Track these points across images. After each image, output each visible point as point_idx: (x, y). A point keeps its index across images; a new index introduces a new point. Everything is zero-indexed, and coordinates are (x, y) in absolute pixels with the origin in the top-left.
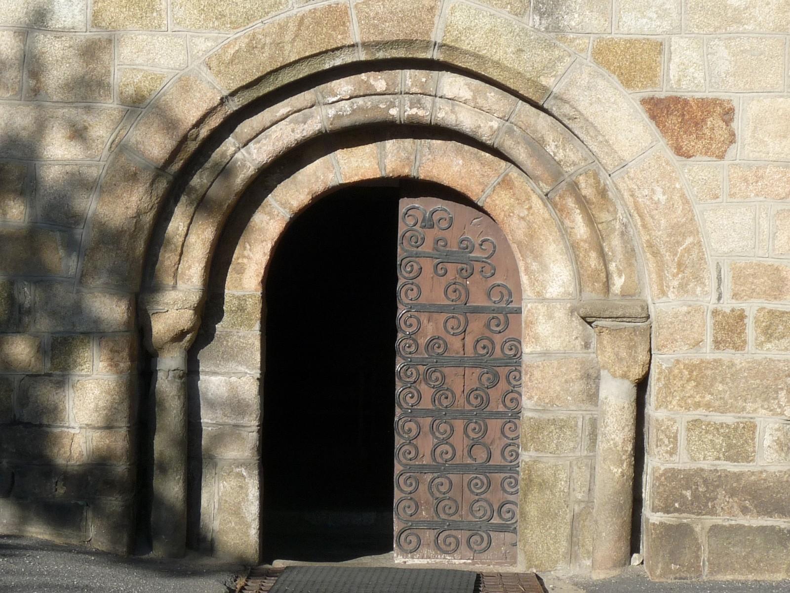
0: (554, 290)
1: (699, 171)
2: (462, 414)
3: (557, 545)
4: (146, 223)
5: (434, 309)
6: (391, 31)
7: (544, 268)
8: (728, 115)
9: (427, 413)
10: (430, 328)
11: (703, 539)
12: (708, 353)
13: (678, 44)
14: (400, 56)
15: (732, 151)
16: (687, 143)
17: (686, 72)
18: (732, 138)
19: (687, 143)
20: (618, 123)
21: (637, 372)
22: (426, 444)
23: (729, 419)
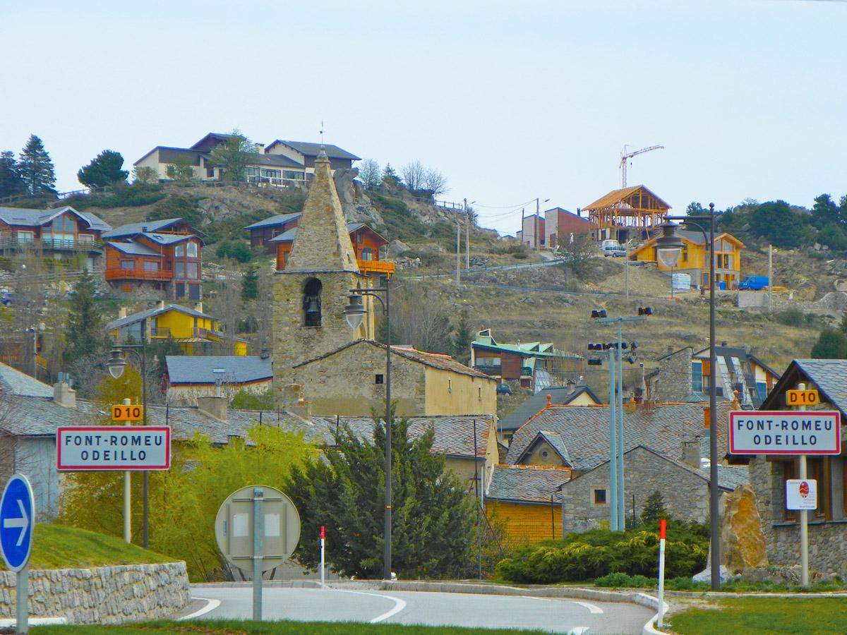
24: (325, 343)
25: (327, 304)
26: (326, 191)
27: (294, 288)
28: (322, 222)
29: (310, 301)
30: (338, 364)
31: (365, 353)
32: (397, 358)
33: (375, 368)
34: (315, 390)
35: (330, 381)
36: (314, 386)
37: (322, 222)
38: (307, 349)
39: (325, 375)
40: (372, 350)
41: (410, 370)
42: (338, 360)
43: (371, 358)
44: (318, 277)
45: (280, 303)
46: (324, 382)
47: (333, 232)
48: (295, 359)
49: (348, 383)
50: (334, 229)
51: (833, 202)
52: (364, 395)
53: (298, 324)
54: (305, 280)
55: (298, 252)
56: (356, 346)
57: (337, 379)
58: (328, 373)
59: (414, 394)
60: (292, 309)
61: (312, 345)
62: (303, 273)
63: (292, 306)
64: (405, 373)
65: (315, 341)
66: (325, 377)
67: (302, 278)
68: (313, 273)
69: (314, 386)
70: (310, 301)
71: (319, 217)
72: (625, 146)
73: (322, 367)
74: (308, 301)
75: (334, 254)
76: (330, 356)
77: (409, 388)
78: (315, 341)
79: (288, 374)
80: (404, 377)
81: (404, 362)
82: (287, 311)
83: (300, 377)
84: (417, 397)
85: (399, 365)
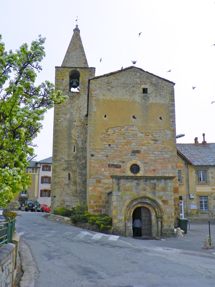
0: (154, 215)
1: (166, 206)
2: (146, 225)
3: (104, 101)
4: (109, 216)
5: (144, 216)
6: (143, 195)
7: (153, 213)
8: (168, 201)
9: (144, 225)
10: (144, 218)
11: (167, 234)
12: (167, 220)
13: (164, 196)
14: (142, 230)
15: (168, 204)
16: (165, 204)
17: (164, 198)
18: (168, 203)
19: (165, 204)
20: (161, 203)
21: (161, 221)
22: (144, 227)
23: (169, 225)
24: (81, 100)
25: (83, 82)
26: (79, 40)
27: (66, 74)
28: (78, 51)
29: (73, 81)
30: (118, 80)
31: (136, 75)
32: (156, 79)
33: (142, 84)
34: (104, 95)
35: (114, 90)
36: (103, 92)
37: (78, 51)
38: (72, 102)
39: (110, 86)
40: (140, 73)
41: (165, 87)
42: (118, 77)
43: (140, 78)
44: (78, 70)
45: (59, 80)
46: (109, 90)
47: (83, 55)
48: (66, 106)
49: (125, 91)
50: (84, 54)
51: (195, 170)
52: (136, 100)
53: (68, 90)
54: (72, 71)
55: (67, 62)
56: (130, 70)
57: (118, 88)
58: (112, 84)
59: (168, 101)
60: (65, 83)
61: (74, 100)
62: (71, 68)
63: (65, 82)
64: (162, 88)
65: (76, 99)
66: (110, 87)
67: (70, 70)
68: (76, 68)
69: (103, 92)
70: (73, 81)
71: (76, 49)
72: (40, 272)
73: (108, 81)
74: (72, 81)
75: (84, 63)
76: (113, 75)
77: (165, 98)
78: (76, 99)
79: (61, 113)
80: (161, 91)
81: (161, 82)
82: (62, 84)
83: (94, 86)
84: (170, 103)
85: (158, 83)
